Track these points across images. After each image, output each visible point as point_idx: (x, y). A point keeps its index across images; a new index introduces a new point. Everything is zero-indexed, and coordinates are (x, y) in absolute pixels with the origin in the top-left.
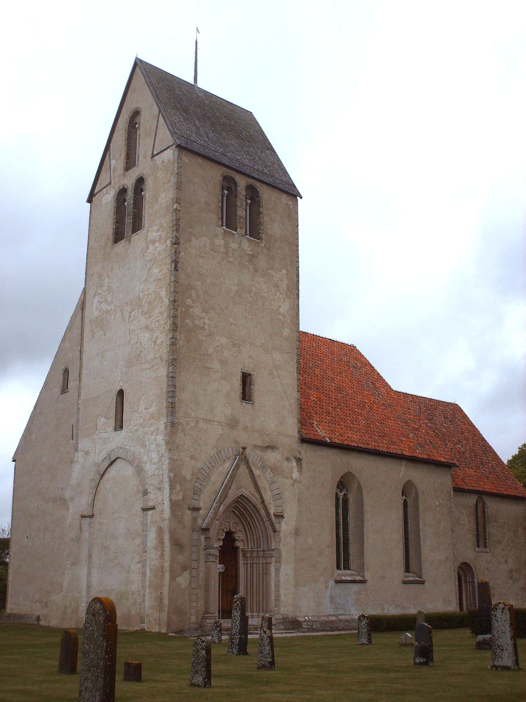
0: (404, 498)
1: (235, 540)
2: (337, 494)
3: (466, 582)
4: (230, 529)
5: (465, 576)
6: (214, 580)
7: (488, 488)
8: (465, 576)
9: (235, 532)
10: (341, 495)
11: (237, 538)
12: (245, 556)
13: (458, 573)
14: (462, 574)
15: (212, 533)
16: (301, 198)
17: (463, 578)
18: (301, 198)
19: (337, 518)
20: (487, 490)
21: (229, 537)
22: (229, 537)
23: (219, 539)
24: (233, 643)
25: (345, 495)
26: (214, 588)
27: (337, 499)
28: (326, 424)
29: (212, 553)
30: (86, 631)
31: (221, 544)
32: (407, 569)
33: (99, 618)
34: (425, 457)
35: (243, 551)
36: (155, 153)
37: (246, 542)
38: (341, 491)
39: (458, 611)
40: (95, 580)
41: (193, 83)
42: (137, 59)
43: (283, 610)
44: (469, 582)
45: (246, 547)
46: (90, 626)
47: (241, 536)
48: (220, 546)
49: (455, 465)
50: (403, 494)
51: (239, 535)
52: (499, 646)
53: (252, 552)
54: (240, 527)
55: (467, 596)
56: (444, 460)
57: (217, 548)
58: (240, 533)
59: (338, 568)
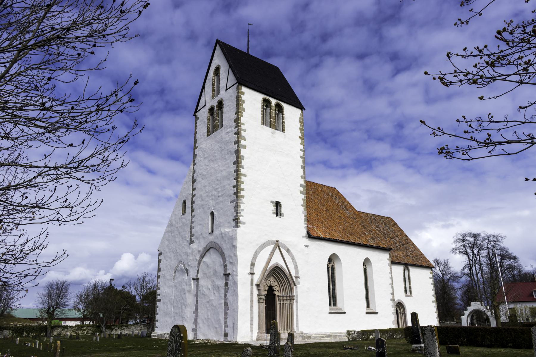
0: (365, 267)
1: (274, 290)
2: (328, 265)
3: (400, 313)
4: (271, 285)
5: (400, 310)
6: (263, 313)
7: (410, 261)
8: (400, 310)
9: (274, 286)
10: (330, 266)
11: (275, 290)
12: (279, 300)
13: (396, 308)
14: (398, 309)
15: (262, 288)
16: (305, 110)
17: (399, 311)
18: (305, 110)
19: (334, 296)
20: (410, 263)
21: (271, 289)
22: (271, 289)
23: (265, 290)
24: (271, 349)
25: (332, 266)
26: (263, 317)
27: (328, 268)
28: (321, 228)
29: (261, 298)
30: (169, 347)
31: (266, 292)
32: (368, 306)
33: (176, 338)
34: (375, 245)
35: (278, 296)
36: (227, 88)
37: (280, 292)
38: (330, 264)
39: (397, 328)
40: (78, 315)
41: (247, 52)
42: (217, 40)
43: (301, 330)
44: (402, 313)
45: (280, 294)
46: (171, 344)
47: (277, 288)
48: (266, 294)
49: (392, 249)
50: (364, 265)
51: (276, 288)
52: (429, 353)
53: (283, 297)
54: (276, 283)
55: (401, 321)
56: (386, 247)
57: (264, 295)
58: (276, 286)
59: (330, 305)
